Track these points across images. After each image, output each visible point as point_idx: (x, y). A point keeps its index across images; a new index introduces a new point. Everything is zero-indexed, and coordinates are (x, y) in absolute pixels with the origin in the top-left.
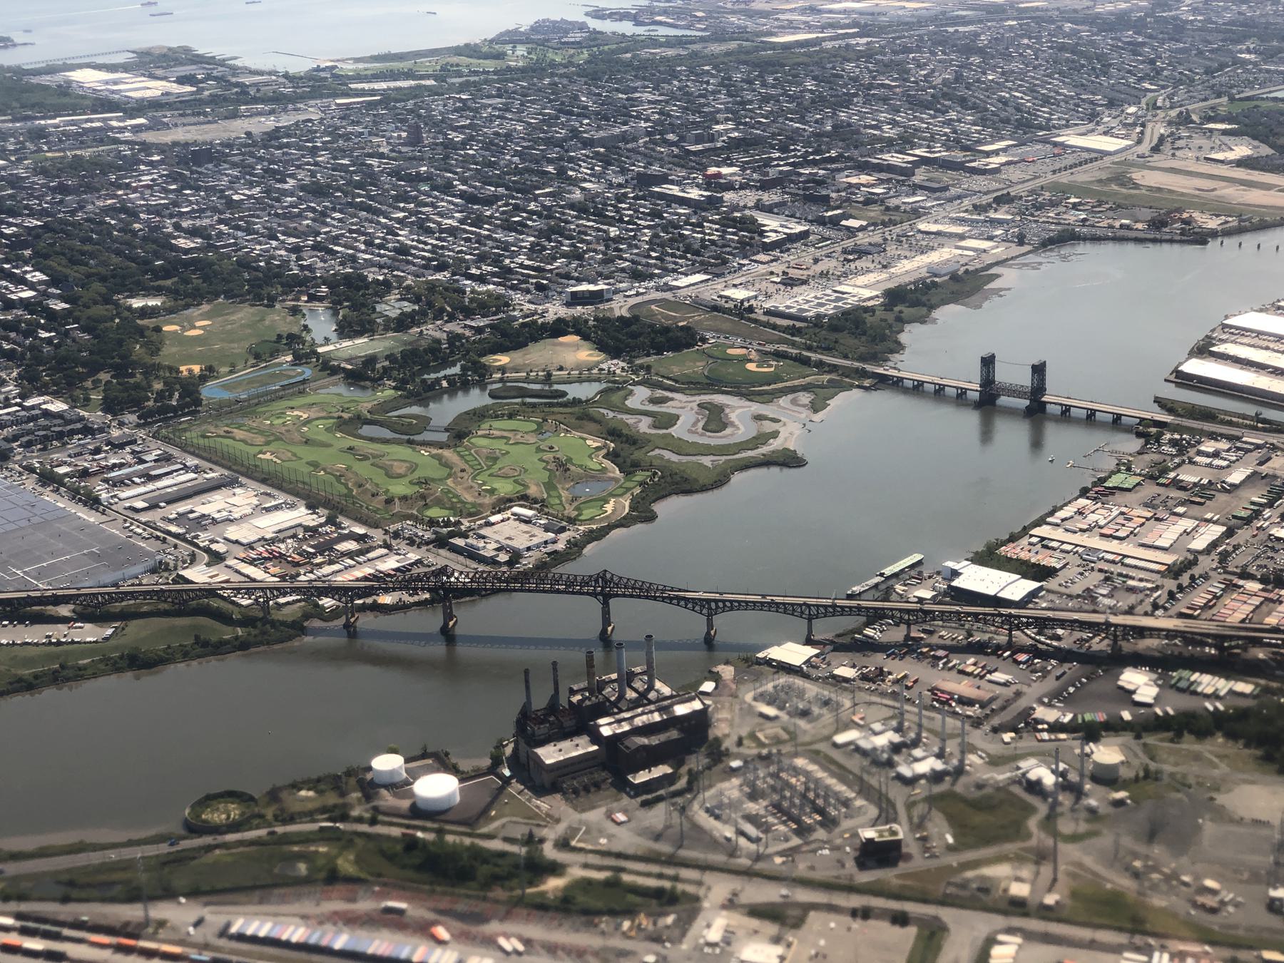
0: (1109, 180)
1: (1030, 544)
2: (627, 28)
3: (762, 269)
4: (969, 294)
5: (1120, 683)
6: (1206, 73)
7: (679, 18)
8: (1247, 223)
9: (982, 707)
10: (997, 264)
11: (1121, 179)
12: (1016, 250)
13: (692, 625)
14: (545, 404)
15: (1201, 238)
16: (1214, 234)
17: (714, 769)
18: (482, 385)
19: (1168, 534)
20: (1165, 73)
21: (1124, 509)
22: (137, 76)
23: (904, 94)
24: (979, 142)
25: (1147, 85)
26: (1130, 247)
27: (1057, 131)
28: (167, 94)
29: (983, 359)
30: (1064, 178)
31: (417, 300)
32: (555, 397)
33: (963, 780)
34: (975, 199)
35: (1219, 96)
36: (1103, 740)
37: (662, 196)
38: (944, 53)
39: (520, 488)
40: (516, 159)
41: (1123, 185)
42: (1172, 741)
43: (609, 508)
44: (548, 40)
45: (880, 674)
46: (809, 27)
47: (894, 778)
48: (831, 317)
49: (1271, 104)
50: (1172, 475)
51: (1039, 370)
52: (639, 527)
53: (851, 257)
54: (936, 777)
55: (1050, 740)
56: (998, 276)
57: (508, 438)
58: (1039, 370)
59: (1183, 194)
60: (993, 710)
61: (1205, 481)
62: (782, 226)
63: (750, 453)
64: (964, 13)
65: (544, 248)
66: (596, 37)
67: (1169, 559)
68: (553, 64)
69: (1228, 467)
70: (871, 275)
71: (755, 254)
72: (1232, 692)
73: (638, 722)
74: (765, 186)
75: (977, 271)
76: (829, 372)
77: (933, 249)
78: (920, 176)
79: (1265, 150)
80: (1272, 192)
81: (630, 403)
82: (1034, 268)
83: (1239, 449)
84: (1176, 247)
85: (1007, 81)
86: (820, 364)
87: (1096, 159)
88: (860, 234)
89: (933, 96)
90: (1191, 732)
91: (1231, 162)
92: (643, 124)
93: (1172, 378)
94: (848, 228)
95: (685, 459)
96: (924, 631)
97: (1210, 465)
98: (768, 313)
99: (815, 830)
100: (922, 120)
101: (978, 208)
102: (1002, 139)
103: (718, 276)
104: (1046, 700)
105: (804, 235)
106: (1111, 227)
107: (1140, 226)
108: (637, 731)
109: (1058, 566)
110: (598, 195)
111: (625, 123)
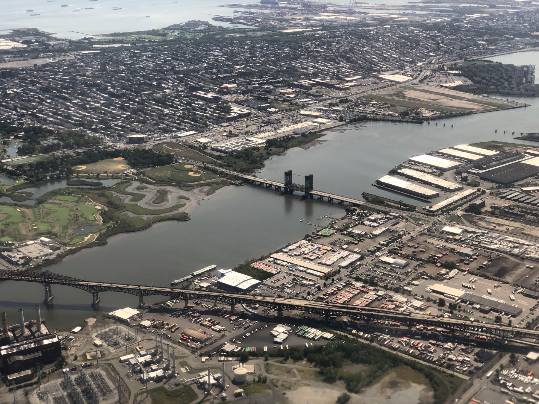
0: (394, 94)
1: (269, 262)
2: (226, 25)
3: (222, 129)
4: (307, 143)
5: (272, 332)
6: (460, 49)
7: (250, 22)
8: (444, 115)
9: (201, 343)
10: (327, 129)
11: (400, 94)
12: (338, 123)
13: (87, 298)
14: (87, 188)
15: (419, 120)
16: (427, 119)
17: (56, 372)
18: (67, 178)
19: (332, 258)
20: (442, 49)
21: (320, 246)
22: (7, 40)
23: (324, 55)
24: (347, 77)
25: (432, 54)
26: (390, 124)
27: (382, 73)
28: (15, 48)
29: (286, 173)
30: (375, 93)
31: (61, 139)
32: (97, 185)
33: (172, 381)
34: (331, 101)
35: (461, 59)
36: (250, 361)
37: (196, 96)
38: (351, 38)
39: (50, 228)
40: (142, 78)
41: (399, 97)
42: (281, 362)
43: (86, 239)
44: (190, 29)
45: (162, 325)
46: (302, 26)
47: (138, 380)
48: (239, 152)
49: (482, 63)
50: (350, 229)
51: (309, 179)
52: (97, 248)
53: (263, 125)
54: (158, 379)
55: (224, 361)
56: (324, 135)
57: (61, 204)
58: (309, 179)
59: (423, 101)
60: (206, 345)
61: (363, 233)
62: (240, 110)
63: (167, 214)
64: (370, 22)
65: (132, 118)
66: (210, 27)
67: (326, 270)
68: (186, 39)
69: (378, 226)
70: (268, 133)
71: (222, 123)
72: (322, 337)
73: (22, 348)
74: (244, 93)
75: (315, 132)
76: (224, 177)
77: (302, 122)
78: (313, 90)
79: (469, 82)
80: (463, 101)
81: (127, 190)
82: (342, 132)
83: (386, 218)
84: (409, 124)
85: (371, 51)
86: (222, 173)
87: (393, 85)
88: (274, 115)
89: (336, 56)
90: (292, 358)
91: (451, 88)
92: (205, 65)
93: (375, 184)
94: (270, 112)
95: (136, 216)
96: (196, 303)
97: (370, 226)
98: (213, 149)
99: (329, 366)
100: (327, 66)
101: (331, 105)
102: (358, 75)
103: (200, 132)
104: (234, 340)
105: (249, 114)
106: (384, 114)
107: (397, 115)
108: (20, 353)
109: (274, 272)
110: (169, 95)
111: (197, 64)
